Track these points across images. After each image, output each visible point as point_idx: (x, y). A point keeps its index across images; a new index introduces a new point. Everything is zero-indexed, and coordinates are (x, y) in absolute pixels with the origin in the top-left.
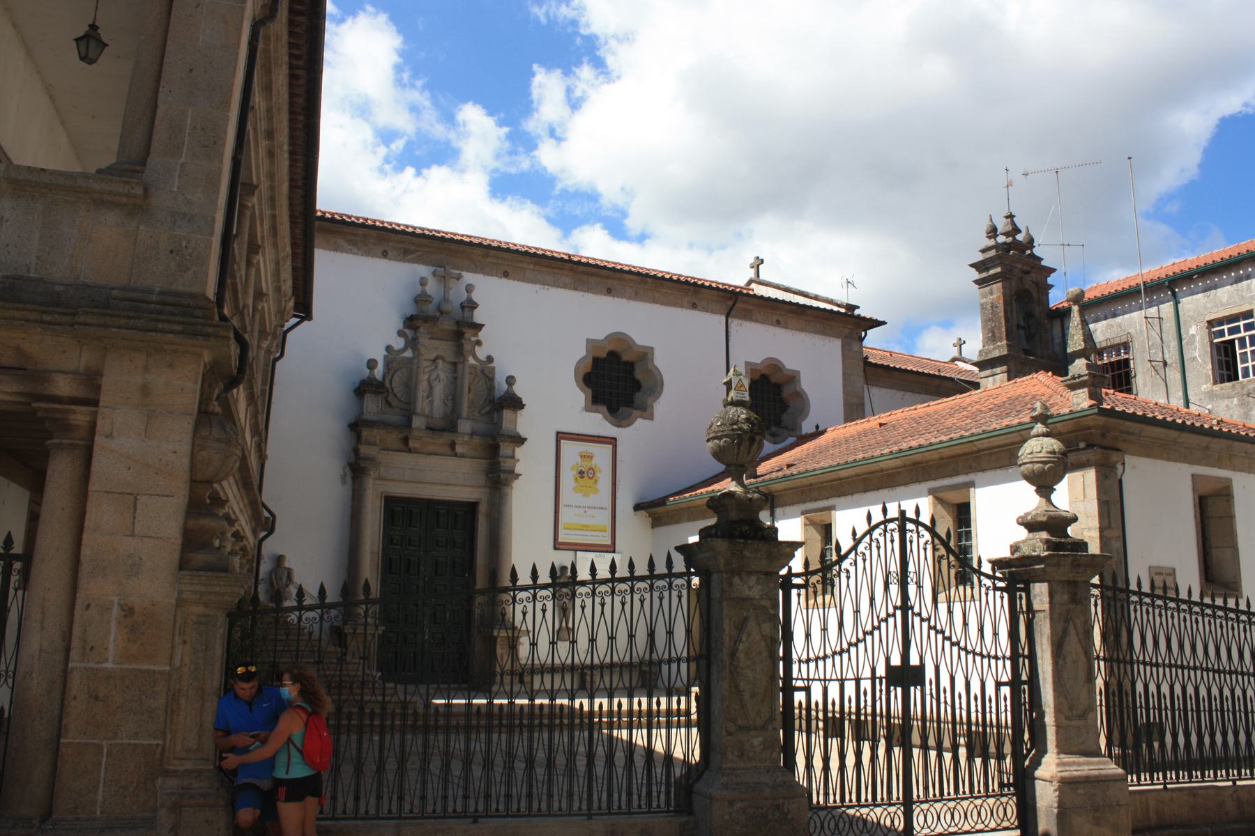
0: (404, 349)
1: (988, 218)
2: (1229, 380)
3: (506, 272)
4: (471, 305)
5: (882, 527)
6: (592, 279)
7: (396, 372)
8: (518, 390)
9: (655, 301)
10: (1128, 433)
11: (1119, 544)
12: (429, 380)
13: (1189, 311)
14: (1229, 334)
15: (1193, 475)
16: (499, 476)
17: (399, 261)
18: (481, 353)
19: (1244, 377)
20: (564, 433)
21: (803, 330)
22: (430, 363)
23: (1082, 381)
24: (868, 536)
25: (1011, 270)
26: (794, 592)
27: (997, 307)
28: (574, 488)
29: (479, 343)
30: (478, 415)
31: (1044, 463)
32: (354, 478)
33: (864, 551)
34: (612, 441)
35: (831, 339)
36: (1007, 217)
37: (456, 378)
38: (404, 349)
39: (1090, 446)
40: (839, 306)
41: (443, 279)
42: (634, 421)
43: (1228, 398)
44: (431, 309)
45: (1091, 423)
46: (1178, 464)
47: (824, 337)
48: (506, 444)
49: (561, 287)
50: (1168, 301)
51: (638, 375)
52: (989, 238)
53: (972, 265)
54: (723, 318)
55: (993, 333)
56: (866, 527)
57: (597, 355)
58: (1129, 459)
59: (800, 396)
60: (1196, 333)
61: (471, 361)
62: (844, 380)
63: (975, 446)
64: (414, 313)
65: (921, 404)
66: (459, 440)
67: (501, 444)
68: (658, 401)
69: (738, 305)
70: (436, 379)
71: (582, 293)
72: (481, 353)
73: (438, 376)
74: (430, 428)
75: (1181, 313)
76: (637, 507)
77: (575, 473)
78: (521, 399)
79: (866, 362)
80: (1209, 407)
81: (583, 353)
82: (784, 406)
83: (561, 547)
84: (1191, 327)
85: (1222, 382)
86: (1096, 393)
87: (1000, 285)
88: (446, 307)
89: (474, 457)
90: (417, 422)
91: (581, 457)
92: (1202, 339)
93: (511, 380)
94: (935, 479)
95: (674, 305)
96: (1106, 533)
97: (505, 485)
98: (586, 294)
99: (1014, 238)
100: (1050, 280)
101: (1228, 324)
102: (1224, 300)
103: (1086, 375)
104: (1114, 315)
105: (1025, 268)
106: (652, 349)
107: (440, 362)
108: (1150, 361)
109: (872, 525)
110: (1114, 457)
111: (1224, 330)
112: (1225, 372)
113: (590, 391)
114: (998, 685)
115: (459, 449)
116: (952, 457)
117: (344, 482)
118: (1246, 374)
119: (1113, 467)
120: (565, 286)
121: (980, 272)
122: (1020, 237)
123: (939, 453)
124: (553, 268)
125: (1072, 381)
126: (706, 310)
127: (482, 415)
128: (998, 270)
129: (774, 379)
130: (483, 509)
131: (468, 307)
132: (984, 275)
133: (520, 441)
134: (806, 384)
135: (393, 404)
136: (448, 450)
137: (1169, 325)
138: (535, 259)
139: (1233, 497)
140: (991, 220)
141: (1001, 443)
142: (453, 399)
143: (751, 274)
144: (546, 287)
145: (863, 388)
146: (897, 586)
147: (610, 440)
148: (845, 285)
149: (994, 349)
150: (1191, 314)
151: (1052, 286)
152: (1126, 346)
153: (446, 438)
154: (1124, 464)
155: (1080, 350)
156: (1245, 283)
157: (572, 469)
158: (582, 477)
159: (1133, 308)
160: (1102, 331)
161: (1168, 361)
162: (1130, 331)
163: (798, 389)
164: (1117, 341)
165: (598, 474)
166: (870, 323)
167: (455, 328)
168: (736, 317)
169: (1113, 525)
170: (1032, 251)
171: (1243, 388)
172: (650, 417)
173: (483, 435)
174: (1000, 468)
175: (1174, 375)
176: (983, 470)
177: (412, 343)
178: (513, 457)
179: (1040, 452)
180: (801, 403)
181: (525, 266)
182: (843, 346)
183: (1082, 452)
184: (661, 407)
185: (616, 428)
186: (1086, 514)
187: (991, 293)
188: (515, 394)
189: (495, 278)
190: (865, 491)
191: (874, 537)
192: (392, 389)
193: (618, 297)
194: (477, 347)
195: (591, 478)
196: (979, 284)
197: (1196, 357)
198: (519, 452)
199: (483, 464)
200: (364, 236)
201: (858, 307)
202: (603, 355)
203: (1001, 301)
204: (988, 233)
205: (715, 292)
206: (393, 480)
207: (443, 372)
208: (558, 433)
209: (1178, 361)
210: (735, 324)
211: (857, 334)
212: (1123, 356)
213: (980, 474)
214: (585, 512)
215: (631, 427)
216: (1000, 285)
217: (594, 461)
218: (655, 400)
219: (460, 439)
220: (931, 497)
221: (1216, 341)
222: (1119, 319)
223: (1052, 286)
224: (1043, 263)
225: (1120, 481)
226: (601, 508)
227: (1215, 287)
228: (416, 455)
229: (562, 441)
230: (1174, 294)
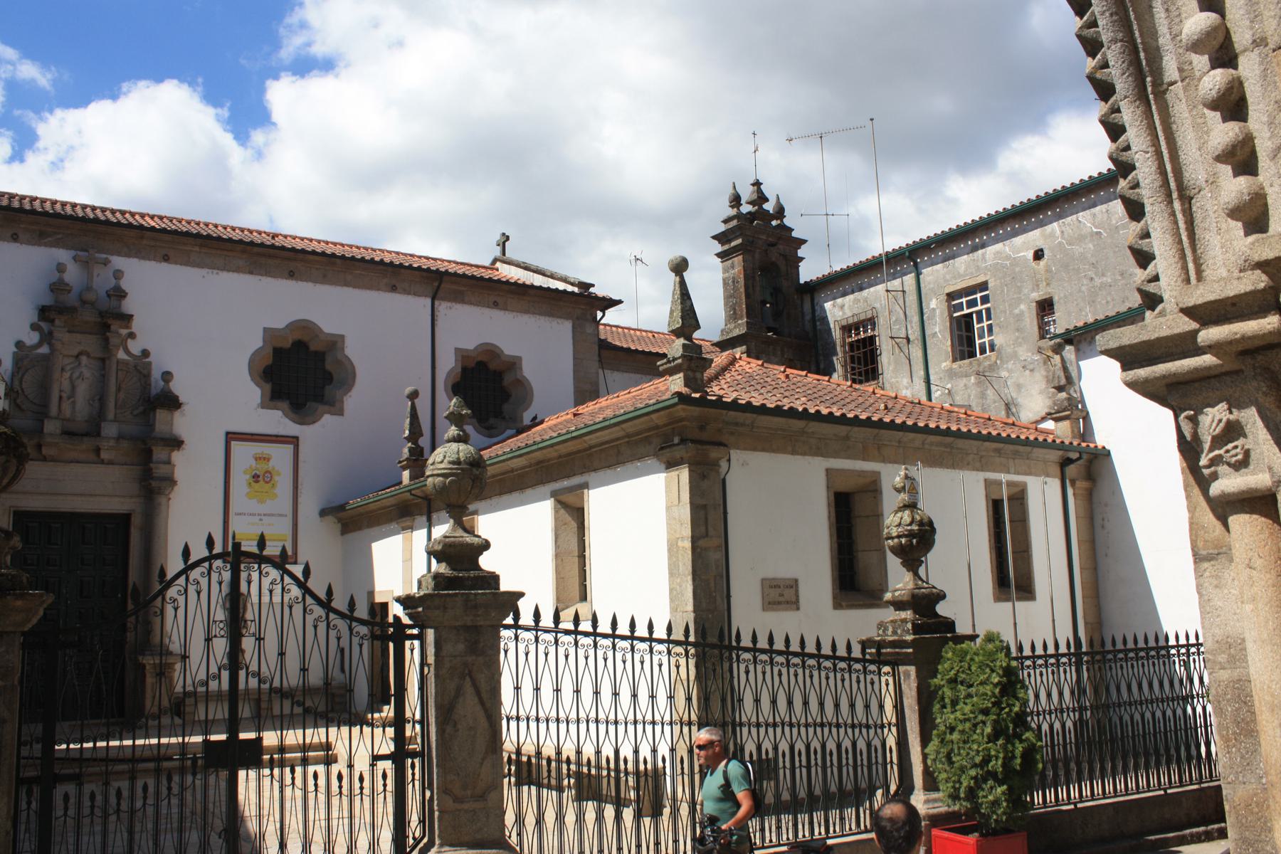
0: (39, 345)
1: (732, 185)
2: (970, 357)
3: (166, 255)
4: (120, 294)
5: (206, 565)
7: (27, 370)
8: (177, 387)
9: (346, 284)
10: (737, 424)
11: (719, 555)
12: (71, 378)
13: (929, 283)
14: (968, 308)
15: (827, 470)
16: (150, 484)
17: (32, 245)
18: (135, 347)
19: (981, 354)
20: (234, 433)
21: (526, 312)
22: (72, 360)
23: (677, 364)
24: (184, 577)
25: (753, 241)
27: (738, 282)
29: (132, 336)
31: (444, 476)
33: (176, 596)
34: (294, 441)
35: (560, 321)
36: (753, 185)
37: (103, 376)
38: (39, 345)
39: (683, 441)
40: (572, 284)
41: (86, 264)
42: (321, 418)
43: (966, 376)
44: (71, 299)
45: (683, 414)
46: (807, 457)
47: (550, 319)
49: (233, 271)
50: (910, 273)
51: (329, 366)
52: (732, 207)
53: (714, 237)
54: (429, 301)
55: (735, 309)
56: (181, 566)
57: (279, 345)
58: (735, 455)
59: (523, 385)
60: (935, 305)
61: (121, 355)
62: (575, 365)
63: (585, 442)
64: (48, 304)
65: (624, 390)
67: (154, 448)
68: (349, 394)
69: (442, 285)
70: (78, 378)
71: (260, 277)
72: (135, 347)
73: (81, 376)
74: (68, 433)
75: (922, 285)
76: (323, 513)
78: (178, 397)
79: (604, 345)
80: (949, 386)
82: (505, 396)
84: (931, 300)
85: (963, 358)
86: (695, 379)
87: (740, 257)
88: (90, 296)
90: (51, 427)
91: (256, 459)
92: (942, 314)
93: (167, 376)
94: (556, 480)
95: (370, 288)
96: (701, 543)
97: (159, 493)
99: (761, 207)
100: (800, 253)
101: (966, 297)
102: (962, 270)
103: (679, 358)
104: (861, 289)
105: (770, 239)
106: (342, 337)
107: (84, 359)
108: (892, 338)
109: (190, 562)
110: (714, 453)
111: (976, 298)
112: (966, 349)
113: (268, 387)
114: (376, 758)
115: (104, 455)
116: (570, 454)
118: (983, 351)
119: (715, 465)
120: (238, 270)
121: (723, 244)
122: (767, 206)
123: (556, 451)
124: (222, 249)
125: (669, 365)
126: (407, 292)
127: (136, 416)
128: (739, 241)
129: (492, 366)
130: (136, 521)
131: (115, 295)
132: (726, 247)
133: (177, 443)
134: (529, 371)
137: (912, 298)
138: (199, 241)
139: (881, 493)
140: (734, 187)
141: (607, 438)
142: (100, 399)
143: (497, 252)
144: (215, 271)
145: (598, 373)
146: (225, 639)
147: (291, 439)
148: (633, 262)
149: (735, 327)
150: (932, 286)
151: (802, 259)
152: (871, 322)
154: (729, 460)
155: (678, 328)
156: (980, 252)
157: (245, 473)
158: (257, 482)
159: (878, 281)
160: (850, 306)
161: (910, 337)
162: (876, 305)
163: (518, 377)
164: (862, 317)
165: (276, 478)
166: (606, 303)
167: (99, 320)
168: (444, 299)
169: (711, 532)
170: (782, 221)
171: (979, 365)
172: (340, 413)
174: (609, 467)
175: (916, 352)
176: (595, 470)
177: (47, 338)
178: (169, 462)
179: (442, 462)
180: (523, 392)
182: (574, 327)
183: (675, 448)
184: (351, 401)
185: (299, 426)
186: (680, 521)
187: (733, 267)
188: (170, 392)
189: (153, 263)
190: (501, 494)
191: (191, 579)
192: (22, 390)
193: (301, 281)
194: (129, 340)
195: (267, 482)
196: (722, 258)
197: (936, 333)
198: (177, 457)
201: (593, 285)
202: (287, 344)
203: (742, 276)
204: (731, 202)
205: (417, 272)
207: (87, 370)
208: (228, 433)
209: (919, 338)
210: (443, 307)
211: (591, 314)
212: (870, 333)
213: (593, 474)
214: (261, 520)
215: (316, 425)
216: (740, 257)
217: (271, 463)
218: (346, 394)
219: (105, 444)
220: (553, 499)
221: (955, 315)
222: (865, 293)
223: (802, 259)
224: (794, 234)
225: (724, 481)
226: (281, 515)
227: (953, 257)
228: (52, 463)
229: (233, 443)
230: (916, 264)
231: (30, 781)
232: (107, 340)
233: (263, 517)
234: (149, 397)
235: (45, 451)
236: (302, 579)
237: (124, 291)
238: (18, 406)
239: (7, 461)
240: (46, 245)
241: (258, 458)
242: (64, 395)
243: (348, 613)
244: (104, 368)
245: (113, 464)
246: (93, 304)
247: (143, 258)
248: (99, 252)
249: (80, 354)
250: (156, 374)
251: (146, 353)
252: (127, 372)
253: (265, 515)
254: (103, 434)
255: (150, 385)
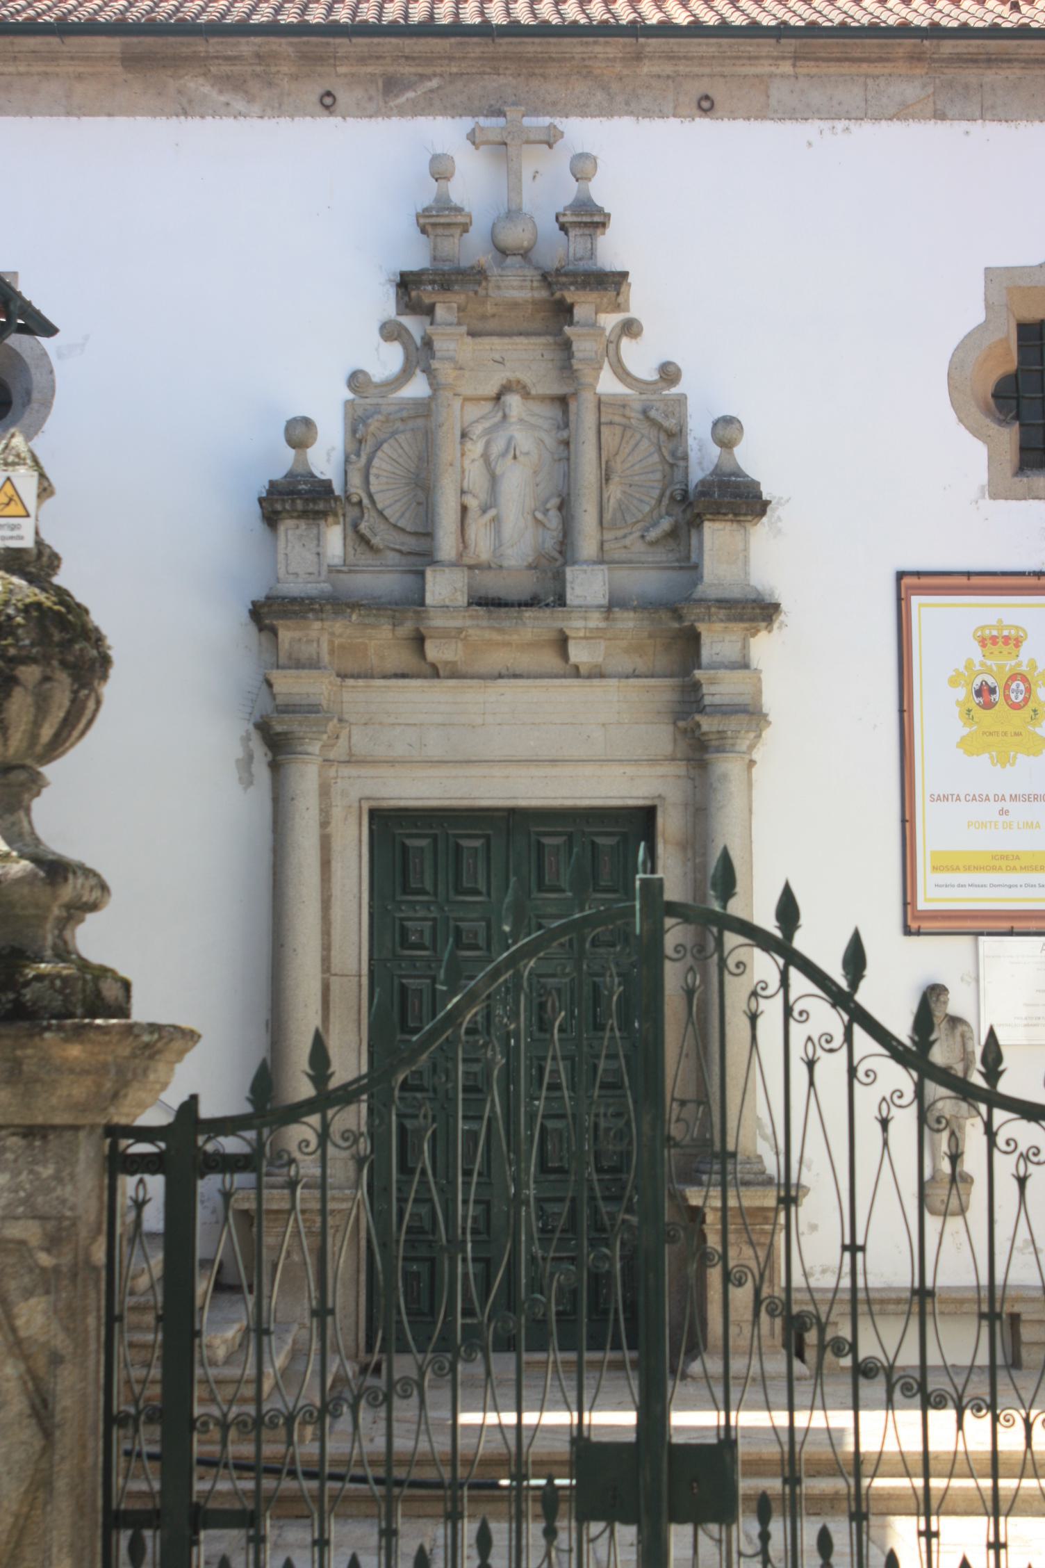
6: (991, 76)
12: (486, 456)
20: (918, 574)
22: (487, 407)
26: (208, 1186)
28: (963, 743)
29: (630, 328)
30: (640, 547)
32: (275, 767)
48: (719, 626)
61: (607, 384)
66: (575, 626)
67: (702, 627)
71: (965, 125)
77: (962, 693)
81: (975, 315)
83: (926, 925)
88: (515, 236)
89: (635, 675)
97: (721, 749)
98: (977, 128)
107: (514, 401)
115: (579, 654)
117: (247, 779)
120: (903, 113)
127: (652, 544)
135: (375, 541)
136: (550, 660)
138: (789, 45)
144: (840, 125)
153: (536, 625)
157: (953, 682)
158: (988, 706)
167: (544, 294)
173: (648, 606)
178: (745, 665)
181: (764, 68)
188: (738, 472)
195: (1015, 706)
199: (662, 691)
200: (259, 57)
206: (392, 763)
208: (901, 575)
217: (1026, 652)
231: (137, 1521)
232: (567, 346)
233: (1007, 805)
234: (685, 492)
235: (434, 651)
236: (843, 983)
237: (600, 211)
238: (364, 540)
239: (46, 679)
240: (402, 112)
241: (987, 641)
242: (472, 503)
243: (778, 934)
244: (567, 425)
245: (602, 676)
246: (525, 254)
247: (647, 113)
248: (535, 112)
249: (505, 389)
250: (698, 430)
251: (669, 374)
252: (625, 427)
253: (1014, 798)
254: (570, 598)
255: (685, 458)
